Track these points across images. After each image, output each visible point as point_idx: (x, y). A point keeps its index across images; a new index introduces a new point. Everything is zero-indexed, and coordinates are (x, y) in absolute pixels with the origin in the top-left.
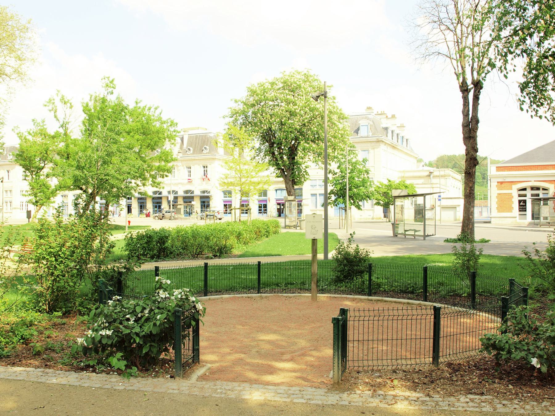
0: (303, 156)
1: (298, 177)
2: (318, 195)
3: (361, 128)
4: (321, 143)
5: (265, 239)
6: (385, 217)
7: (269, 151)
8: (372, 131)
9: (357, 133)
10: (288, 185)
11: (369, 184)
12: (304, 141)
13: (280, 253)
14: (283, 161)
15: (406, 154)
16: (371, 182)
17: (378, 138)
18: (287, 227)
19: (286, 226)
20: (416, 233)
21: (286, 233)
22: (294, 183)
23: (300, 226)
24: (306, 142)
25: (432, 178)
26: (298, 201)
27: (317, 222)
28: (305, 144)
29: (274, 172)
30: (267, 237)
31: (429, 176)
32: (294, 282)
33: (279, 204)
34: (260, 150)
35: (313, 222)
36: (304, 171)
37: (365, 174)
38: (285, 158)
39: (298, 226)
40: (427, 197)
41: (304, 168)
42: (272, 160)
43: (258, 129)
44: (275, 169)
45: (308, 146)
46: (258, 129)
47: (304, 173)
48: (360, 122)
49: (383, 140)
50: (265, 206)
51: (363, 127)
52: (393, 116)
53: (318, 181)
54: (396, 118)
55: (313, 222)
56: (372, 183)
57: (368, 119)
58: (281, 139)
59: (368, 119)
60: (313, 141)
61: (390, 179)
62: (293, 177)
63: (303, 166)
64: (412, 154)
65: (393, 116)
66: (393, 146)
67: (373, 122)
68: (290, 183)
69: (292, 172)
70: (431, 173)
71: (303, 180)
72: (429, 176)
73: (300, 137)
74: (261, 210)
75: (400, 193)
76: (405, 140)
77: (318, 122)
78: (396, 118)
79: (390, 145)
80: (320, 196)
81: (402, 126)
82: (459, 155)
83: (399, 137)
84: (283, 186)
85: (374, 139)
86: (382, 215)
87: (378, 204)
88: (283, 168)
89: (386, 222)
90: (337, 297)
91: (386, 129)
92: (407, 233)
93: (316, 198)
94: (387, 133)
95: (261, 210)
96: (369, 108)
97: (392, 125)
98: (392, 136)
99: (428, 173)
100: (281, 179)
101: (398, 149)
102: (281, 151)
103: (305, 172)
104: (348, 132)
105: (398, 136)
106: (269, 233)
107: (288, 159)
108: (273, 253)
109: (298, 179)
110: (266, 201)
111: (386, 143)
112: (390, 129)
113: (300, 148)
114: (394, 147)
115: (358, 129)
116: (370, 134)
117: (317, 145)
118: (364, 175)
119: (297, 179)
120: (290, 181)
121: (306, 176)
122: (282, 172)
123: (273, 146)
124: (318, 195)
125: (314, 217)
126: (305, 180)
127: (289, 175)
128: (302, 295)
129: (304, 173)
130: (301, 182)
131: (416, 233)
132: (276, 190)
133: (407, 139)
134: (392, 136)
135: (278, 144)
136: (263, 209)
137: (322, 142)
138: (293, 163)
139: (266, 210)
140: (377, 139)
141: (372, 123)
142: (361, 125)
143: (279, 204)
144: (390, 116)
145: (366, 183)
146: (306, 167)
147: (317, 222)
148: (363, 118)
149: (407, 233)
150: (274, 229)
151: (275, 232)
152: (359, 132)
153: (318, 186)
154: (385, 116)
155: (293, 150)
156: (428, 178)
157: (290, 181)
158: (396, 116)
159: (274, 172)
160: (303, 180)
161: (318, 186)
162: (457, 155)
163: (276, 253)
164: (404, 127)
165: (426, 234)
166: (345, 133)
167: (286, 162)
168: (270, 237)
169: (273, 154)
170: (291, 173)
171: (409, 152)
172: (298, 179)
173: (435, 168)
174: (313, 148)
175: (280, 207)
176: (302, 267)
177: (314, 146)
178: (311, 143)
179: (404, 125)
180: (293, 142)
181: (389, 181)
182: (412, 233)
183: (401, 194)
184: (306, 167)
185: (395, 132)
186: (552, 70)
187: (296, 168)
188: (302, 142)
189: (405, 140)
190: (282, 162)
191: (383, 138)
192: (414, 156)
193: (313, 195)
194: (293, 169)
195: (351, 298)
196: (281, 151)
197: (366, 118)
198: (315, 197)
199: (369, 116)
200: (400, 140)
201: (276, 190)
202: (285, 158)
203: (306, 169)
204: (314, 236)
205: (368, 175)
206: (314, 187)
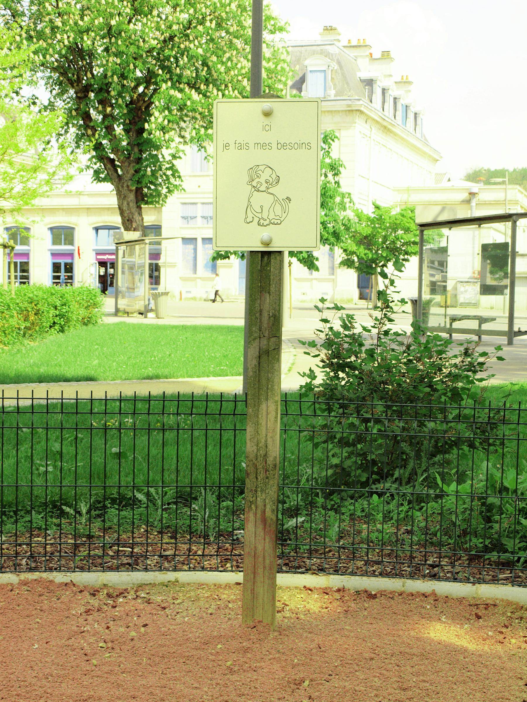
0: (166, 122)
1: (151, 183)
2: (199, 241)
3: (310, 78)
4: (215, 91)
5: (53, 336)
6: (362, 297)
7: (76, 110)
8: (335, 85)
9: (300, 90)
10: (125, 203)
11: (338, 199)
12: (169, 84)
13: (92, 373)
14: (114, 139)
15: (414, 148)
16: (343, 196)
17: (350, 103)
18: (120, 314)
19: (117, 311)
20: (485, 327)
21: (117, 324)
22: (140, 198)
23: (156, 311)
24: (173, 87)
25: (474, 208)
26: (150, 244)
27: (282, 146)
28: (172, 92)
29: (88, 167)
30: (62, 331)
31: (468, 201)
32: (140, 496)
33: (102, 264)
34: (51, 107)
35: (264, 146)
36: (168, 166)
37: (330, 175)
38: (119, 130)
39: (151, 310)
40: (521, 222)
41: (168, 158)
42: (83, 135)
43: (45, 45)
44: (90, 160)
45: (179, 95)
46: (45, 45)
47: (169, 173)
48: (306, 63)
49: (362, 109)
50: (69, 268)
51: (315, 74)
52: (386, 55)
53: (199, 206)
54: (392, 59)
55: (264, 146)
56: (346, 200)
57: (327, 55)
58: (109, 74)
59: (327, 55)
60: (193, 86)
61: (379, 203)
62: (139, 182)
63: (166, 153)
64: (426, 149)
65: (386, 55)
66: (385, 127)
67: (339, 63)
68: (132, 197)
69: (137, 167)
70: (472, 194)
71: (164, 191)
72: (468, 201)
73: (160, 72)
74: (58, 277)
75: (438, 216)
76: (411, 116)
77: (208, 34)
78: (392, 59)
79: (377, 122)
80: (203, 243)
81: (405, 82)
82: (515, 170)
83: (399, 106)
84: (113, 201)
85: (341, 106)
86: (356, 292)
87: (348, 263)
88: (112, 156)
89: (368, 309)
90: (382, 593)
91: (370, 83)
92: (456, 325)
93: (195, 250)
94: (371, 92)
95: (58, 277)
96: (329, 29)
97: (385, 75)
98: (384, 102)
99: (465, 196)
100: (108, 187)
101: (395, 134)
102: (109, 109)
103: (172, 168)
104: (285, 66)
105: (395, 103)
106: (68, 320)
107: (127, 131)
108: (70, 372)
109: (153, 187)
110: (71, 255)
111: (368, 119)
112: (378, 83)
113: (158, 102)
114: (386, 129)
115: (302, 80)
116: (332, 93)
117: (205, 95)
118: (326, 176)
119: (149, 188)
120: (131, 191)
121: (172, 180)
122: (109, 166)
123: (86, 96)
124: (199, 241)
125: (267, 114)
126: (170, 191)
127: (129, 176)
128: (184, 576)
129: (169, 173)
130: (159, 195)
131: (485, 327)
132: (97, 229)
133: (416, 114)
134: (384, 102)
135: (101, 90)
136: (63, 274)
137: (218, 90)
138: (138, 145)
139: (71, 278)
140: (349, 106)
141: (336, 67)
142: (309, 69)
143: (102, 264)
144: (377, 55)
145: (331, 197)
146: (174, 157)
147: (282, 146)
148: (314, 53)
149: (456, 325)
150: (83, 312)
151: (87, 322)
152: (304, 86)
153: (199, 219)
154: (368, 53)
155: (140, 109)
156: (466, 206)
157: (131, 191)
158: (392, 55)
159: (88, 167)
160: (164, 191)
161: (199, 219)
162: (511, 170)
163: (80, 372)
164: (410, 83)
165: (516, 329)
166: (279, 68)
167: (120, 140)
168: (71, 331)
169: (87, 117)
170: (132, 171)
171: (419, 145)
172: (153, 187)
173: (482, 184)
174: (193, 102)
175: (106, 270)
176: (171, 420)
177: (195, 95)
178: (187, 89)
179: (410, 79)
180: (141, 89)
181: (377, 207)
182: (474, 325)
183: (442, 218)
184: (174, 157)
185: (390, 92)
186: (3, 506)
187: (146, 159)
188: (164, 86)
189: (411, 116)
190: (110, 141)
191: (363, 104)
192: (430, 156)
193: (187, 240)
194: (139, 160)
195: (461, 600)
196: (109, 109)
197: (322, 52)
198: (192, 247)
199: (331, 49)
200: (400, 113)
201: (97, 229)
202: (119, 130)
203: (174, 162)
204: (265, 233)
205: (337, 179)
206: (191, 221)
